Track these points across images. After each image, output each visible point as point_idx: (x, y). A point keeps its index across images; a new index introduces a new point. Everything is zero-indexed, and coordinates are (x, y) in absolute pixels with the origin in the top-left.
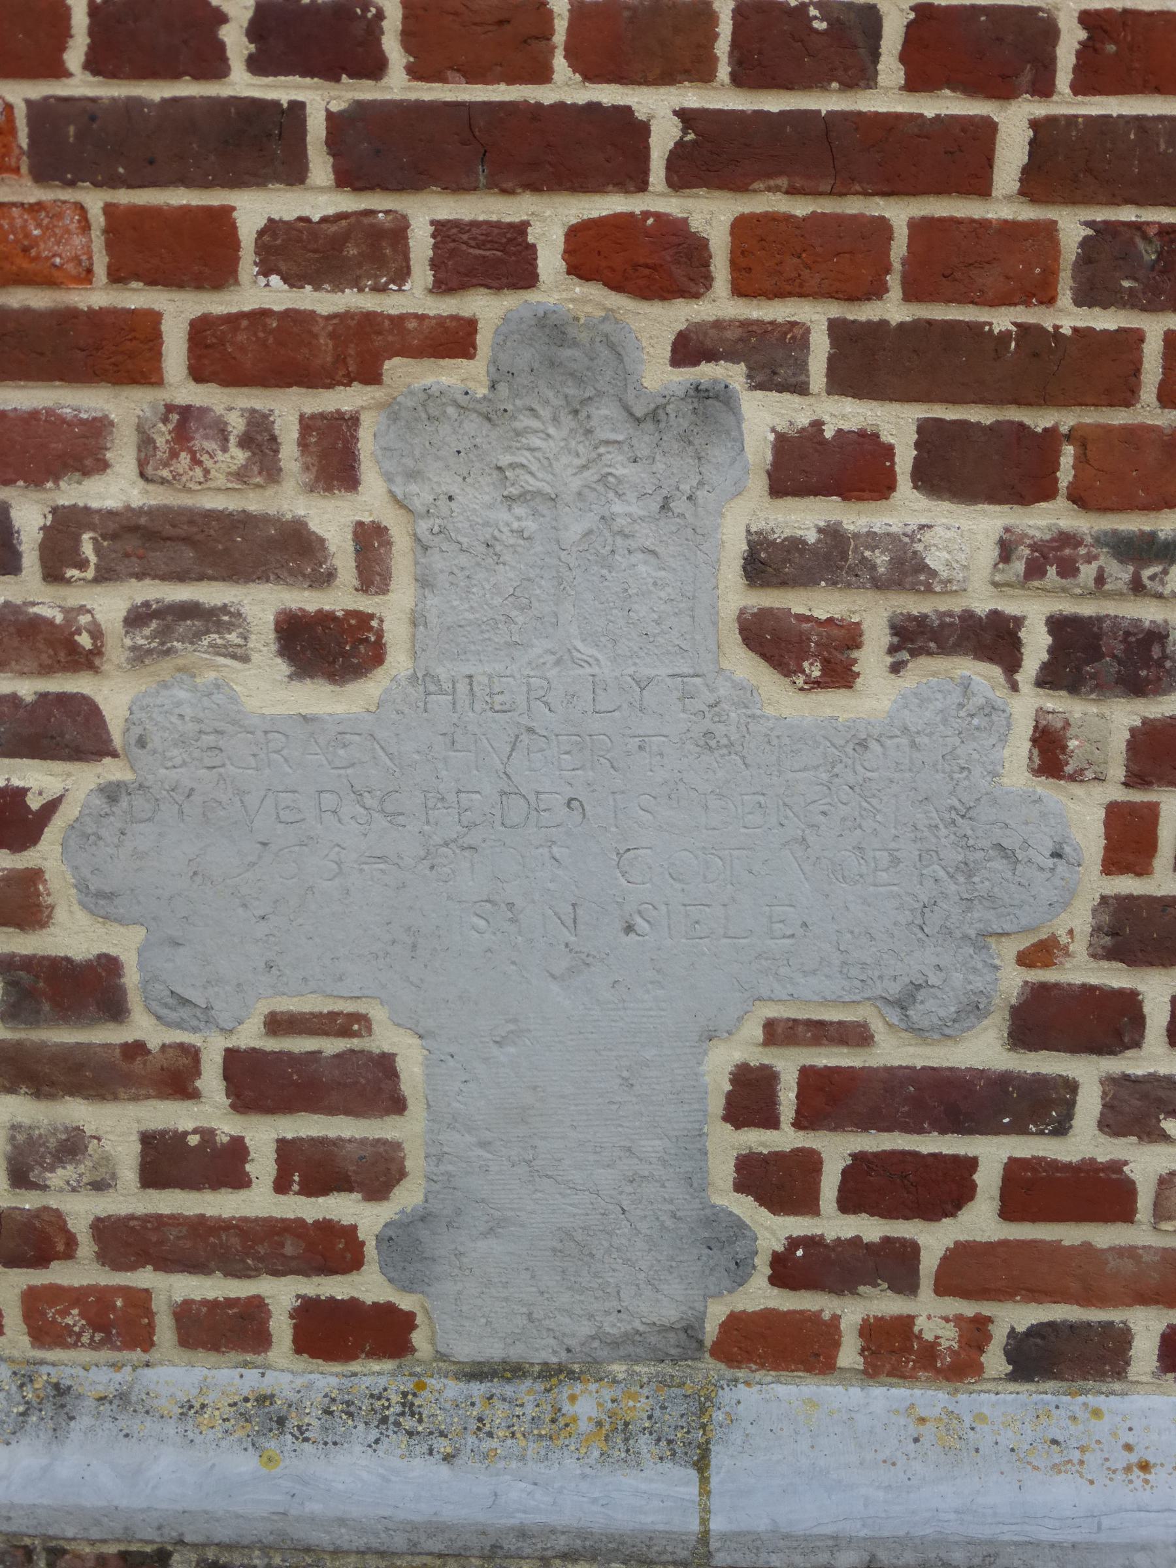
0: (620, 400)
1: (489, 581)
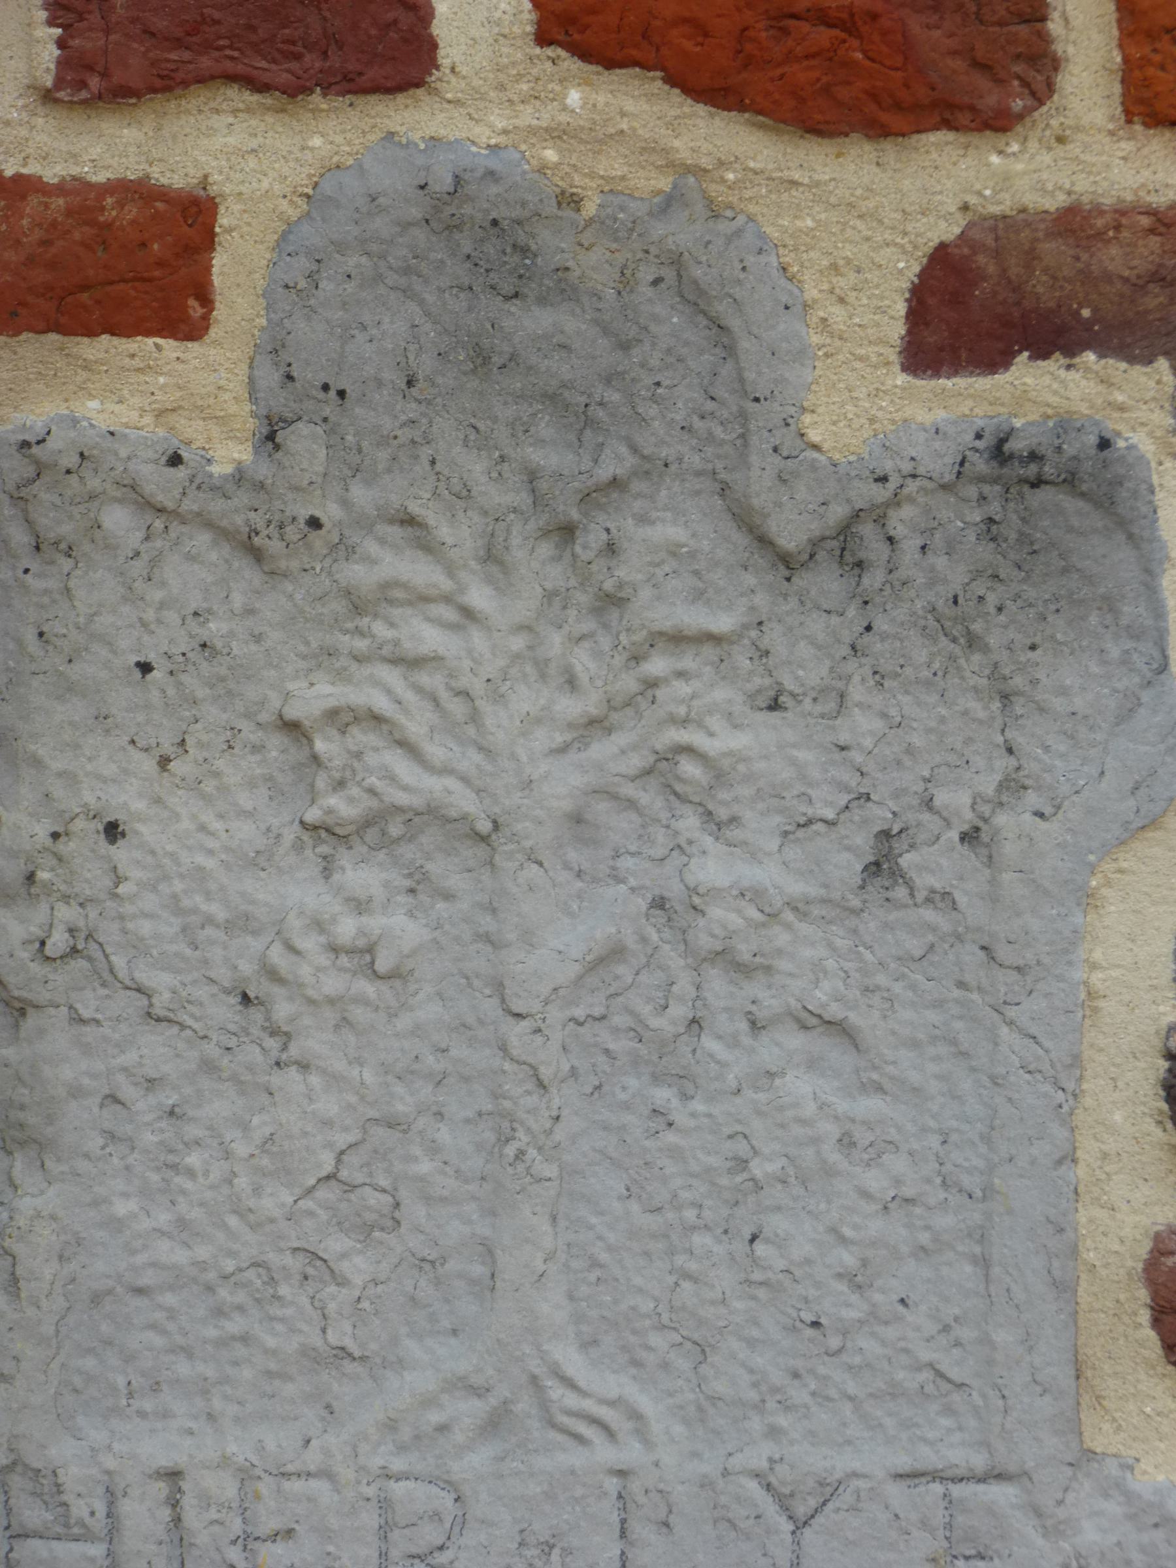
0: (724, 490)
1: (245, 1127)
